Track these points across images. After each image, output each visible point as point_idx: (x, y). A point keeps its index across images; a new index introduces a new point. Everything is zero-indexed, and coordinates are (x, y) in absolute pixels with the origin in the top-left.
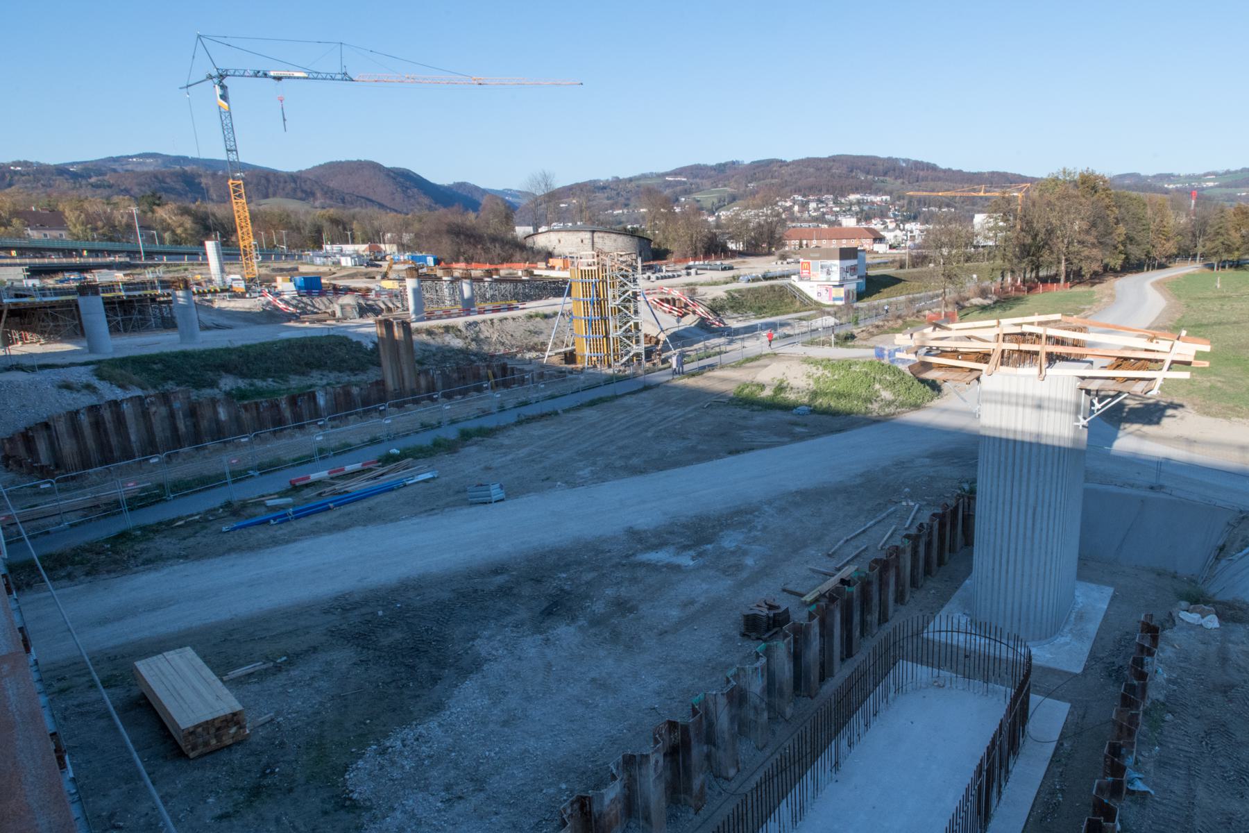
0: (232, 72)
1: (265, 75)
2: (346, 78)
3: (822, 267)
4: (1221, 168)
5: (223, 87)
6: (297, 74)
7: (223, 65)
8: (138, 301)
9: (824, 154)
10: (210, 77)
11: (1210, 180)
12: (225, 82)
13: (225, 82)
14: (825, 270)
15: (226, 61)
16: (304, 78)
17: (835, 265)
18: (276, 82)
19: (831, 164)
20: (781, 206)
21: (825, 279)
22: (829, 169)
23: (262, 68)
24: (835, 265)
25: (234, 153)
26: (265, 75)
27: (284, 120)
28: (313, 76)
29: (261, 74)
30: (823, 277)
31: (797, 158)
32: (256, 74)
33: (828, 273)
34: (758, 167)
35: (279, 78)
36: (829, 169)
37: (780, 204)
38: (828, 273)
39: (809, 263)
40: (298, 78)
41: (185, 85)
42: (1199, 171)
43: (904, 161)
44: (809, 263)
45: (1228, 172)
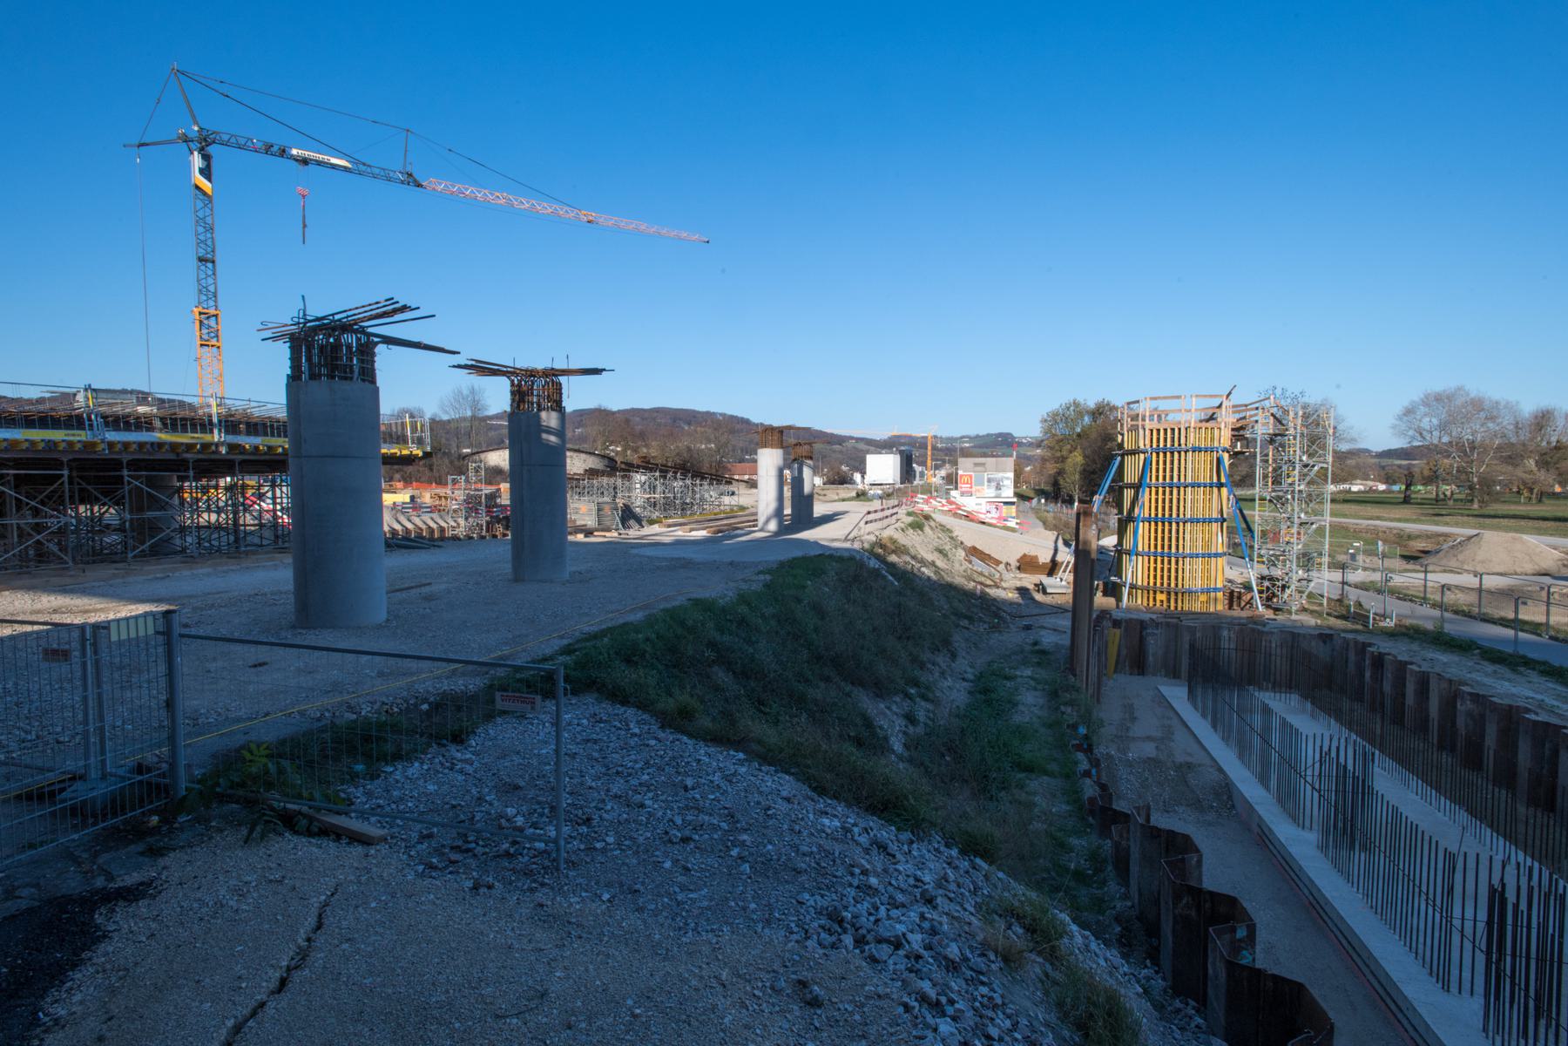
0: (225, 137)
1: (283, 153)
2: (412, 181)
3: (989, 481)
4: (973, 433)
5: (206, 158)
6: (334, 161)
7: (210, 126)
8: (135, 465)
9: (647, 406)
10: (186, 139)
11: (966, 442)
12: (211, 150)
13: (211, 150)
14: (994, 484)
15: (219, 119)
16: (345, 169)
17: (1007, 478)
18: (300, 167)
19: (655, 414)
20: (613, 451)
21: (993, 495)
22: (654, 419)
23: (278, 142)
24: (1007, 478)
25: (210, 265)
26: (283, 153)
27: (305, 226)
28: (360, 169)
29: (275, 149)
30: (991, 492)
31: (621, 408)
32: (268, 149)
33: (998, 487)
34: (581, 415)
35: (305, 162)
36: (654, 419)
37: (611, 448)
38: (998, 487)
39: (971, 476)
40: (334, 166)
41: (137, 143)
42: (957, 434)
43: (721, 414)
44: (971, 476)
45: (977, 436)
